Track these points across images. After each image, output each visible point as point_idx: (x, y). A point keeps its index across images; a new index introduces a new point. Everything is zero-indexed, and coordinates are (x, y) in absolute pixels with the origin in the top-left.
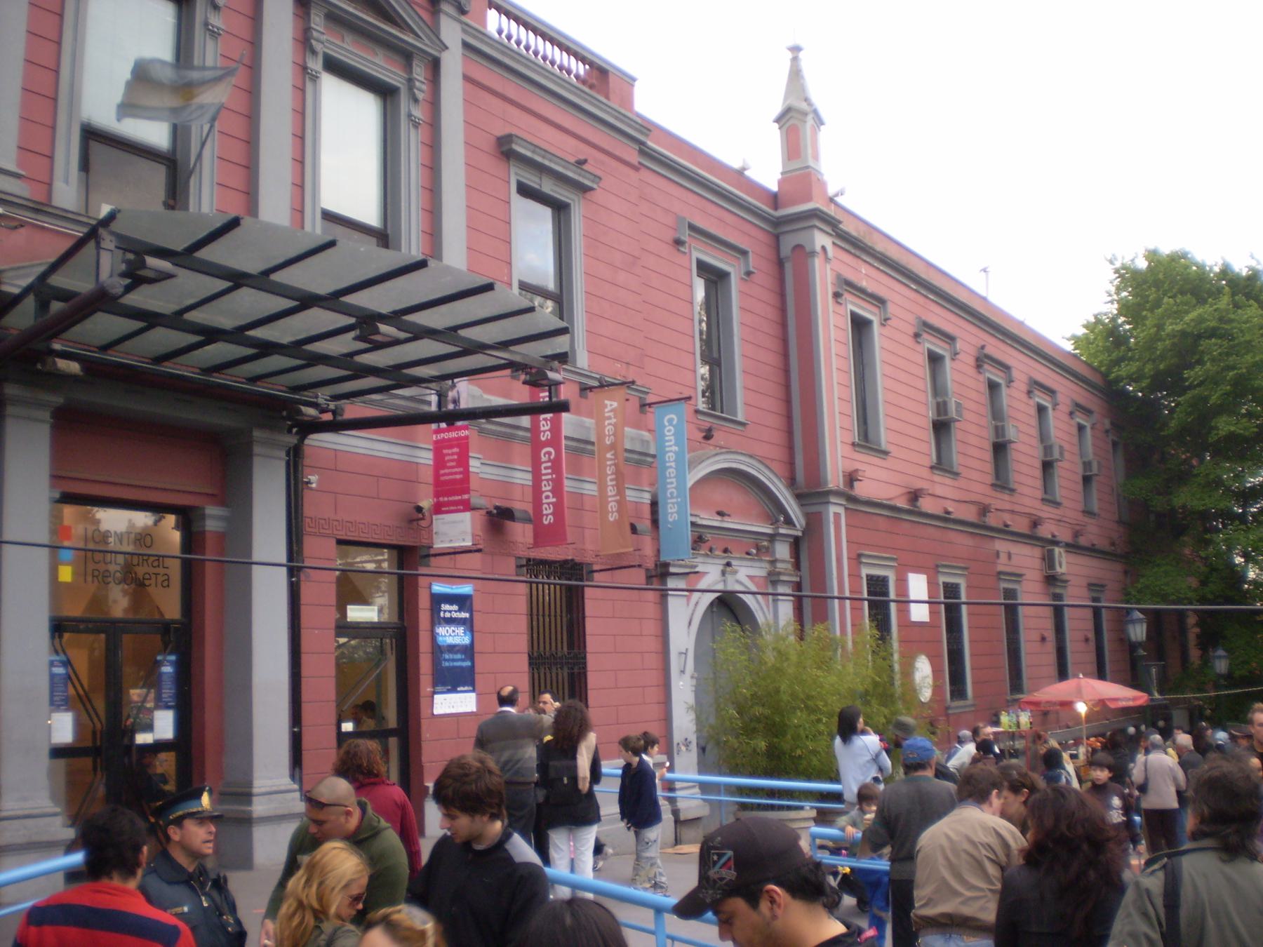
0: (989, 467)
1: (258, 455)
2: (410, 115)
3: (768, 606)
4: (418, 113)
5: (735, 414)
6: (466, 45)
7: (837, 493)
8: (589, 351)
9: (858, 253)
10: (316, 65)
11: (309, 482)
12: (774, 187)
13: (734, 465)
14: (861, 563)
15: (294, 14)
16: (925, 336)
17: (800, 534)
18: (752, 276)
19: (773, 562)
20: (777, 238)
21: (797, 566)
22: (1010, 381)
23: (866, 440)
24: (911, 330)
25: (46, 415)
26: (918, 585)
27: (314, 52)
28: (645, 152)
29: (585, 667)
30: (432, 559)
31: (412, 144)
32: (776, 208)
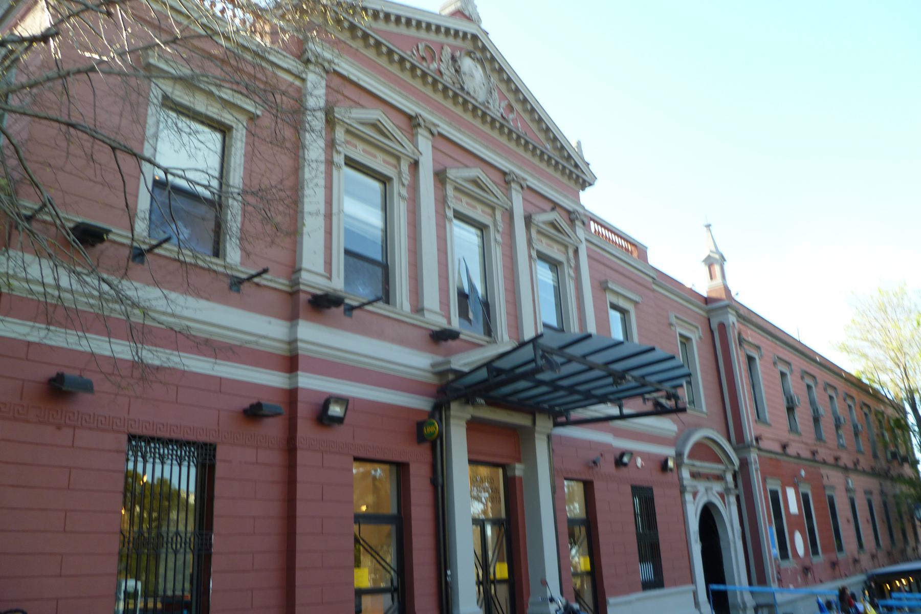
2: (399, 194)
4: (404, 192)
9: (746, 323)
12: (705, 295)
22: (816, 383)
26: (791, 493)
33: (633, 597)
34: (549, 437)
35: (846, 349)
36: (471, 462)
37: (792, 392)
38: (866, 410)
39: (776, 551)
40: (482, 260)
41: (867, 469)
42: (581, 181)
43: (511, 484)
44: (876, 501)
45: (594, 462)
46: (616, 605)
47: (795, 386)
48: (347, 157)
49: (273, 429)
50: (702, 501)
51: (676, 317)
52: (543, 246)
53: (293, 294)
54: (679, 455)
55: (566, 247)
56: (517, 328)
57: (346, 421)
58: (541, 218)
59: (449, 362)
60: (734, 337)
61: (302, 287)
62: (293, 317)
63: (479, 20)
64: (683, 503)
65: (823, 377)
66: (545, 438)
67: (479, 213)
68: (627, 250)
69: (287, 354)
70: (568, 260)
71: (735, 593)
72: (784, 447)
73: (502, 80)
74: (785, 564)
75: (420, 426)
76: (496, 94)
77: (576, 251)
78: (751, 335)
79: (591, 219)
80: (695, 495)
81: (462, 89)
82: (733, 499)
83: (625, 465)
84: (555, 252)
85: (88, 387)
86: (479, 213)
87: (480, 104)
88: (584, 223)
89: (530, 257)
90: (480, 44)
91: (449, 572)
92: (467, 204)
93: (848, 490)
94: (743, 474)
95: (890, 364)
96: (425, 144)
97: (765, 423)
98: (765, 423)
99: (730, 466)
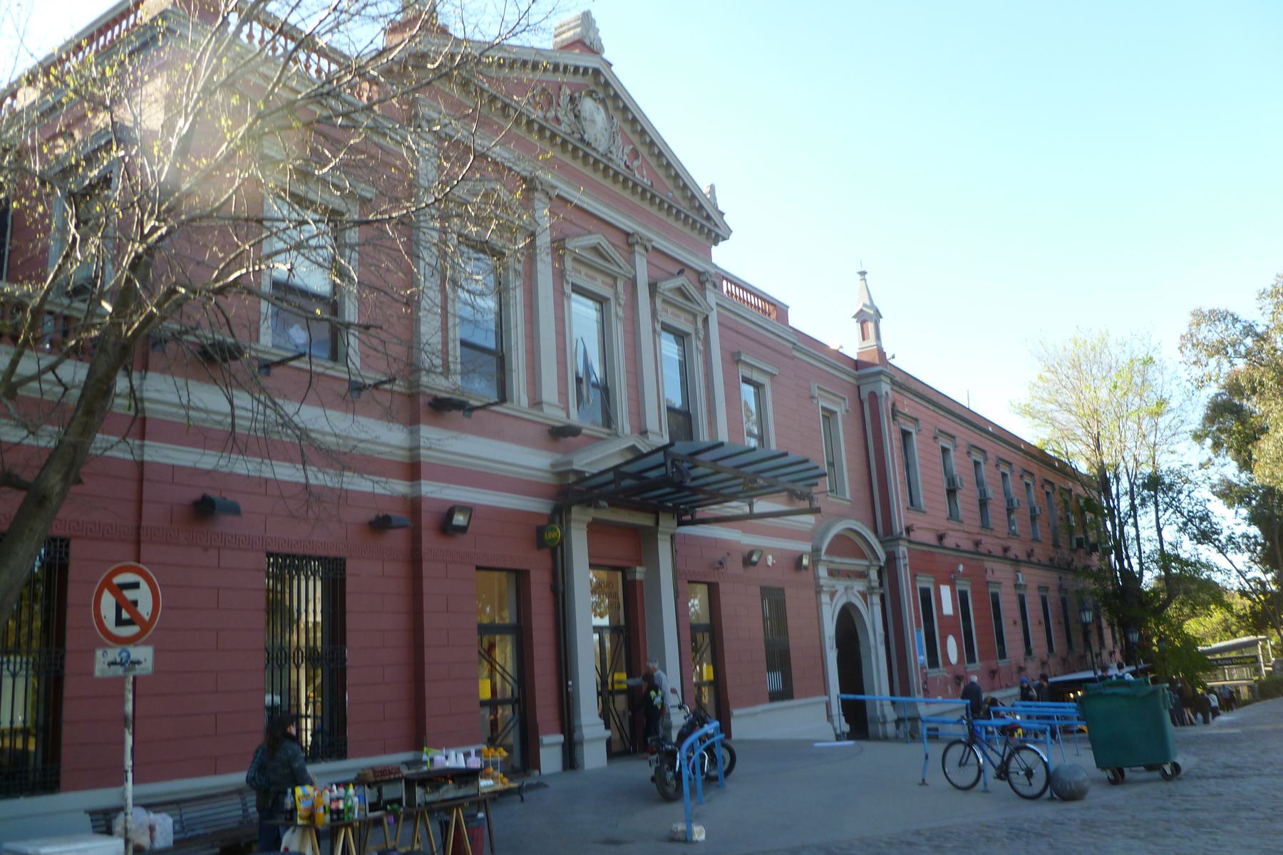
0: (978, 516)
6: (717, 304)
9: (902, 391)
10: (568, 289)
12: (855, 357)
22: (986, 460)
23: (912, 503)
26: (945, 591)
32: (857, 369)
33: (759, 708)
34: (672, 537)
35: (1028, 412)
36: (592, 566)
37: (955, 473)
38: (1048, 488)
39: (923, 658)
40: (601, 339)
41: (1044, 560)
42: (713, 235)
43: (631, 588)
44: (1053, 598)
45: (721, 563)
46: (740, 716)
47: (960, 465)
48: (573, 284)
49: (396, 540)
50: (840, 601)
51: (818, 388)
52: (668, 316)
53: (412, 396)
54: (816, 550)
55: (695, 316)
56: (639, 415)
57: (470, 529)
58: (667, 286)
59: (571, 463)
60: (887, 410)
61: (422, 389)
62: (413, 421)
63: (602, 48)
64: (818, 606)
65: (1018, 460)
66: (669, 538)
67: (599, 285)
68: (764, 311)
69: (407, 460)
70: (696, 330)
71: (874, 703)
72: (941, 538)
73: (625, 120)
74: (933, 673)
75: (540, 531)
76: (619, 140)
77: (706, 320)
78: (908, 405)
79: (724, 278)
80: (832, 595)
81: (582, 140)
82: (876, 599)
83: (754, 564)
84: (683, 323)
85: (234, 510)
86: (599, 285)
87: (602, 155)
88: (715, 286)
89: (654, 331)
90: (602, 80)
91: (570, 683)
92: (586, 275)
93: (1017, 586)
94: (889, 570)
95: (1080, 432)
96: (544, 213)
97: (919, 510)
98: (919, 510)
99: (875, 563)
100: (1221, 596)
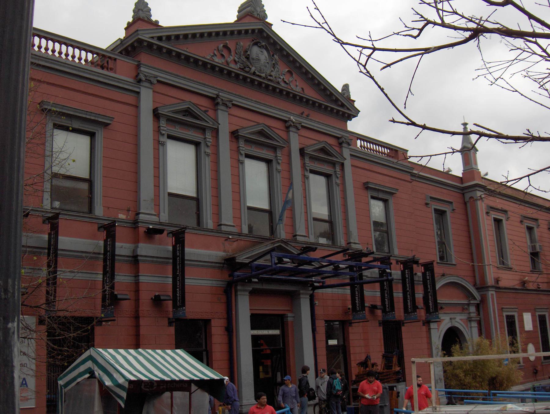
1: (302, 298)
3: (468, 329)
4: (338, 181)
5: (452, 261)
6: (351, 155)
7: (492, 287)
8: (398, 248)
11: (316, 304)
13: (452, 281)
14: (503, 311)
15: (301, 159)
16: (525, 221)
17: (479, 302)
18: (455, 210)
19: (469, 313)
20: (463, 194)
21: (479, 314)
24: (519, 220)
25: (247, 293)
26: (527, 317)
27: (241, 154)
28: (413, 175)
29: (403, 355)
30: (353, 324)
31: (207, 162)
32: (462, 183)
79: (358, 139)
82: (474, 324)
100: (455, 343)
